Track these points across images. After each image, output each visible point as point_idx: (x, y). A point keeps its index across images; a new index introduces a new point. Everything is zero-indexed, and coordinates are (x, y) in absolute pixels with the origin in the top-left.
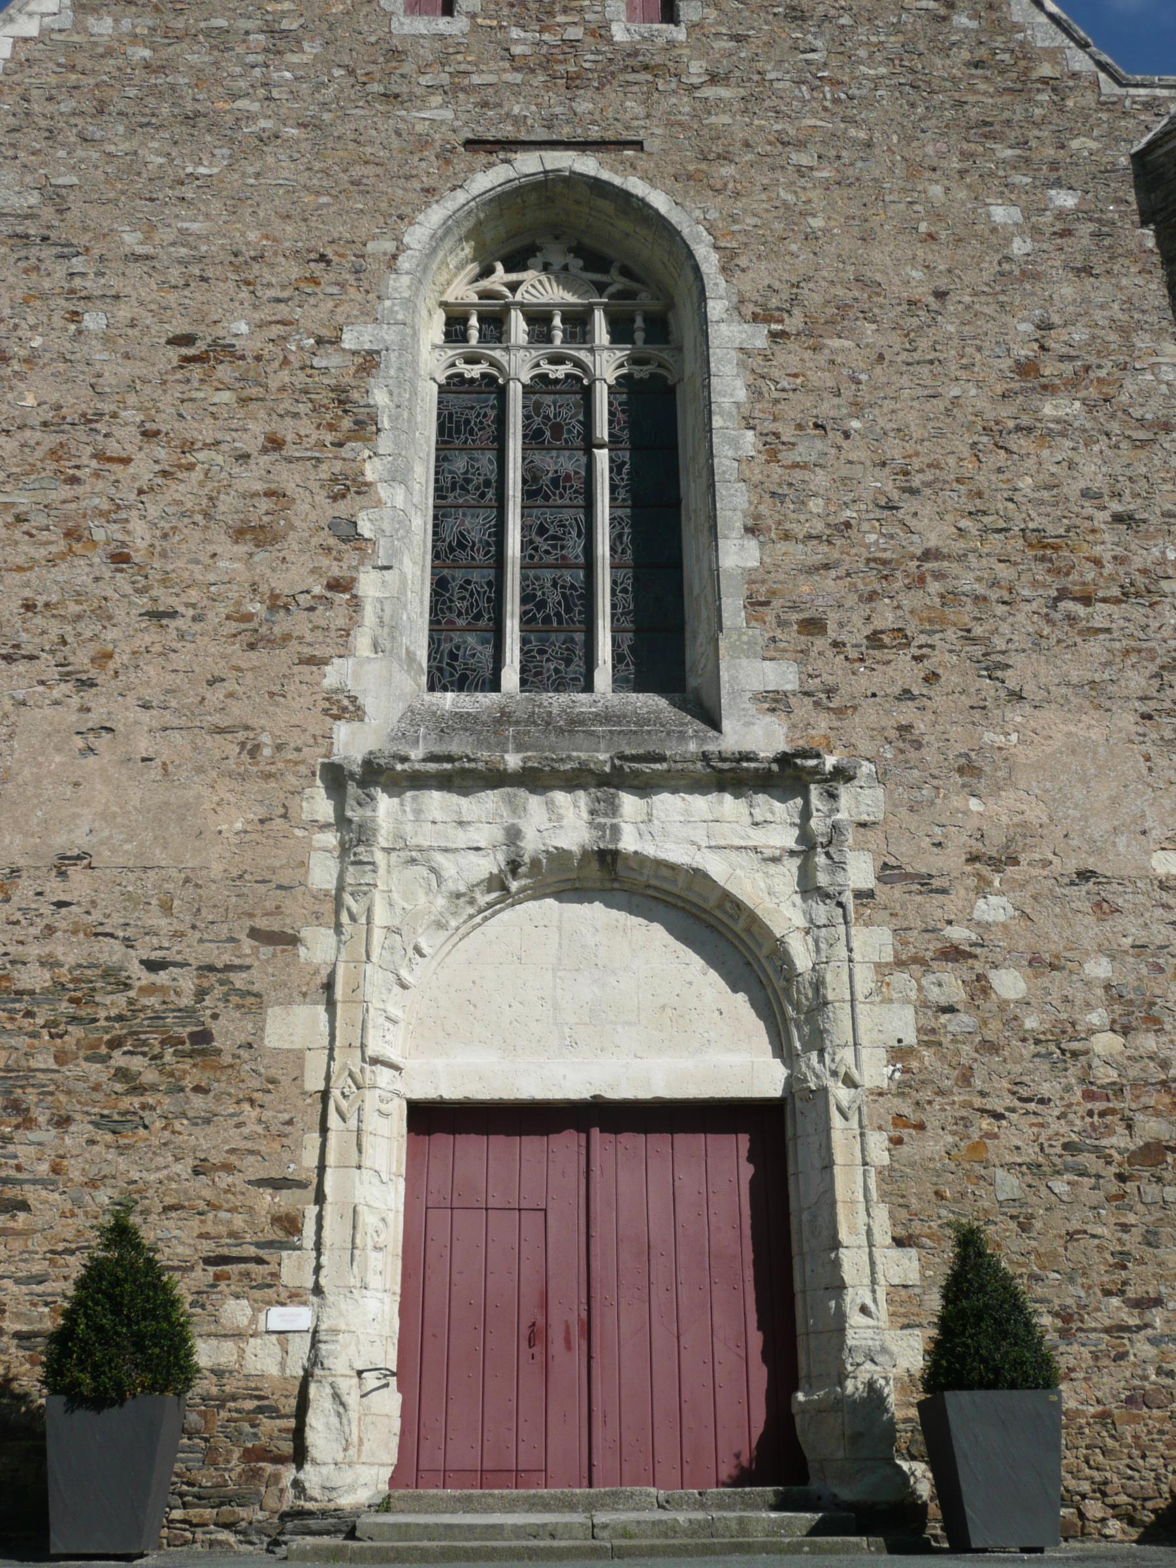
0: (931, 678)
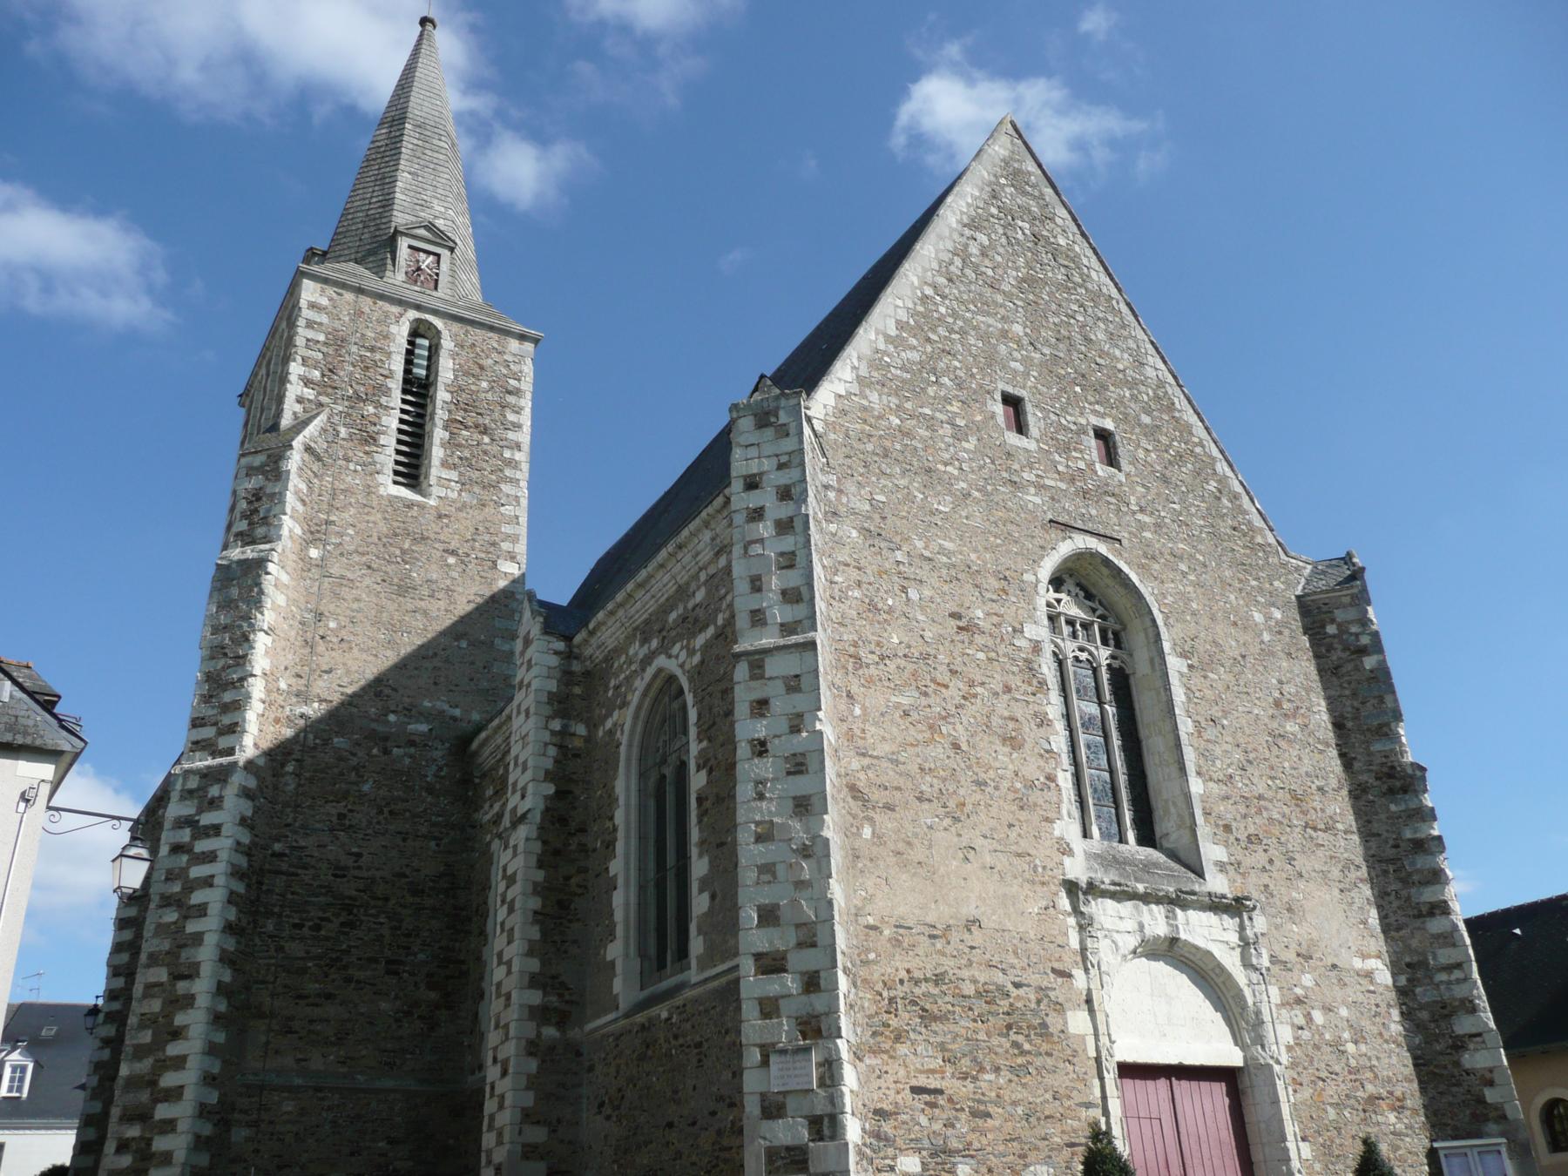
0: (1271, 861)
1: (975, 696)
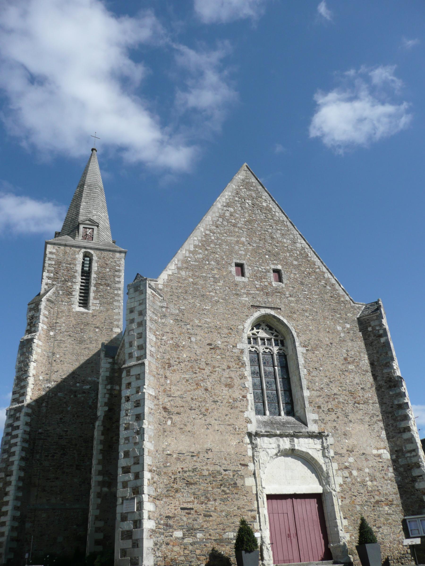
0: (338, 417)
1: (215, 371)
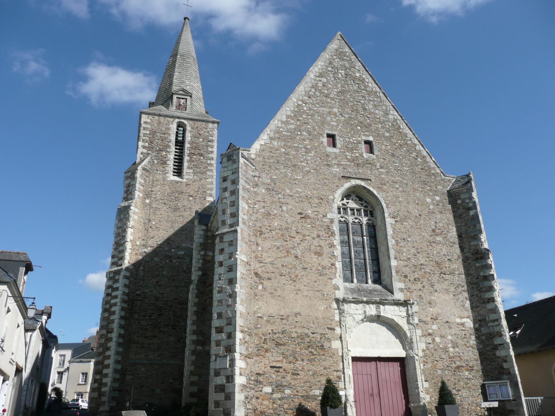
0: (424, 287)
